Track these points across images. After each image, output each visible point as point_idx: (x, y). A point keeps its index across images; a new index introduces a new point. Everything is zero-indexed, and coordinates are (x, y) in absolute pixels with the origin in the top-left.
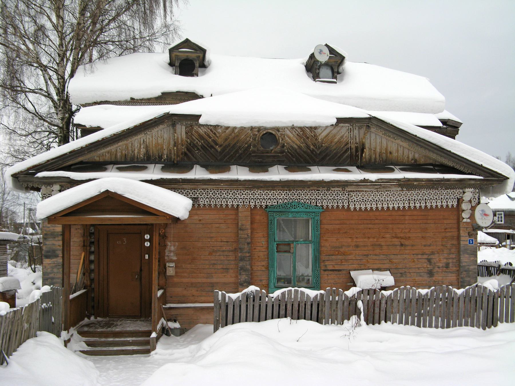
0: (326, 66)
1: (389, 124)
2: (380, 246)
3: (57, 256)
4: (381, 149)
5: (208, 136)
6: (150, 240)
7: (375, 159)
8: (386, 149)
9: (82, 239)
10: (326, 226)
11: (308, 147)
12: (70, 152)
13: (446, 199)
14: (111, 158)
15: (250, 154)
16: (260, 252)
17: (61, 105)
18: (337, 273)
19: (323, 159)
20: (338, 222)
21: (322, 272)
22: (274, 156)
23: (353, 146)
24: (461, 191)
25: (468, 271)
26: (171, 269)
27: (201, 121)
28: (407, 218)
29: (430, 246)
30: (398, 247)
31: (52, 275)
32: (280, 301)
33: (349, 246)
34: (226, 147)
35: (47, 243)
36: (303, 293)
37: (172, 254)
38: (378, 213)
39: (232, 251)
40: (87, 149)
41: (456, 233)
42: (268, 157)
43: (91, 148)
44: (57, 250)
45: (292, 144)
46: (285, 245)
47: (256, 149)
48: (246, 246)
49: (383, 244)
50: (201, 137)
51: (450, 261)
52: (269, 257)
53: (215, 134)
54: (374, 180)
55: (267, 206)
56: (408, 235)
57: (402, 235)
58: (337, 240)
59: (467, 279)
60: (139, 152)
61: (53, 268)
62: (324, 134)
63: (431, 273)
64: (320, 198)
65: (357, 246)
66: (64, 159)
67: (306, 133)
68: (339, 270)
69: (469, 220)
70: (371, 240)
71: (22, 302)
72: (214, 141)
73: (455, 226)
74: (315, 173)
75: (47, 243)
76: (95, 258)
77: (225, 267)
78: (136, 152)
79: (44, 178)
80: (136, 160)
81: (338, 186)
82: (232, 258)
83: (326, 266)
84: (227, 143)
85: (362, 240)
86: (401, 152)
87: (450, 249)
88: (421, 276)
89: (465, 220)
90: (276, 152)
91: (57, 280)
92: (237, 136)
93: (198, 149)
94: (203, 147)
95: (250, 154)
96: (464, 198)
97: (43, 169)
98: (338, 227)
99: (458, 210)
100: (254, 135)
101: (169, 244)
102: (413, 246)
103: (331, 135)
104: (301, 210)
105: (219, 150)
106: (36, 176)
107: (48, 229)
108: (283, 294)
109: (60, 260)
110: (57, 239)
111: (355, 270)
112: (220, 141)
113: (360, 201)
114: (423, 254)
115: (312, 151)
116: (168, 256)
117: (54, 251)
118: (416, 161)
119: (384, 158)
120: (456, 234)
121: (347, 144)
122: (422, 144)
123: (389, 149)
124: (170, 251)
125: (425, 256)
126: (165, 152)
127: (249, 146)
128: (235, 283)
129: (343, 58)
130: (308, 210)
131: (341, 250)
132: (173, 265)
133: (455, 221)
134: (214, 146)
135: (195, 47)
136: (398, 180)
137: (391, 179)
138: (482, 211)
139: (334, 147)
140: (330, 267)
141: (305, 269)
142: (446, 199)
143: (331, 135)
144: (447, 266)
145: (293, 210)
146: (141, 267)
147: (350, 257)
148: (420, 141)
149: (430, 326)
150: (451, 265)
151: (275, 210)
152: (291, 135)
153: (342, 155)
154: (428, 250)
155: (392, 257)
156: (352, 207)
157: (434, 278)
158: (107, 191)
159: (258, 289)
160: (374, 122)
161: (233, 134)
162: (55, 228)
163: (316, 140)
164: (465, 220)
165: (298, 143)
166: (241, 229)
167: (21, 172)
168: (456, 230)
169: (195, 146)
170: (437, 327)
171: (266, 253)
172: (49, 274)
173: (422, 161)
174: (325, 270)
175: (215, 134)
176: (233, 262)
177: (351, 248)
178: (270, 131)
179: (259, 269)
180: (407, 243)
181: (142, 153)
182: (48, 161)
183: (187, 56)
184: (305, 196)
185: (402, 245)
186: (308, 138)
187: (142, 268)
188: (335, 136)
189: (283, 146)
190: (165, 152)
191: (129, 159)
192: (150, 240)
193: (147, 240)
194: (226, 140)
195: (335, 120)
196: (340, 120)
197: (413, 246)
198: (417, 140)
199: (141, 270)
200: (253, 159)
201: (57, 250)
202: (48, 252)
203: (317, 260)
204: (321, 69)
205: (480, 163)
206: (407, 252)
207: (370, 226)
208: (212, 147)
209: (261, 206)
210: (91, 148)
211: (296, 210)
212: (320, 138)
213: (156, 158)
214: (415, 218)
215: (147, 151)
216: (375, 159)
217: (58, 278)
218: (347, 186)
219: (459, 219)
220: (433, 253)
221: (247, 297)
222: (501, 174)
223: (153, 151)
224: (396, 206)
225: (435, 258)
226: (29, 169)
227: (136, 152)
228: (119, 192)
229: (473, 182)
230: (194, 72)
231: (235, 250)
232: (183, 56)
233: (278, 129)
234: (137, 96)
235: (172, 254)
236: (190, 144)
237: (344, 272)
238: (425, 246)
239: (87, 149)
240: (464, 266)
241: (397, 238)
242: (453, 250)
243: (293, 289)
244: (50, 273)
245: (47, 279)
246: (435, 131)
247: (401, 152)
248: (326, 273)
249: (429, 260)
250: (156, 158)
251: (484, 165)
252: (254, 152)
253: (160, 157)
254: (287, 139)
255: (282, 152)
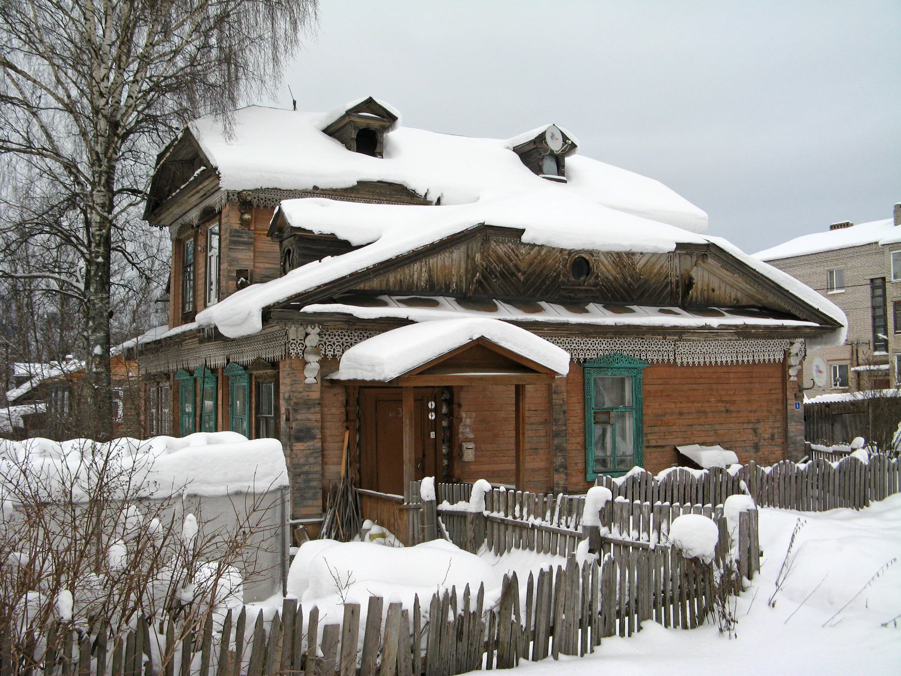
0: (542, 156)
1: (728, 253)
2: (705, 412)
3: (313, 438)
4: (702, 285)
5: (509, 257)
6: (436, 410)
7: (697, 298)
8: (708, 285)
9: (343, 410)
10: (647, 388)
11: (625, 279)
12: (351, 275)
13: (772, 352)
14: (381, 285)
15: (559, 286)
16: (575, 424)
17: (103, 182)
18: (660, 450)
19: (642, 295)
20: (660, 381)
21: (645, 449)
22: (586, 291)
23: (674, 280)
24: (788, 341)
25: (794, 443)
26: (469, 451)
27: (525, 238)
28: (732, 375)
29: (755, 412)
30: (724, 415)
31: (306, 468)
32: (666, 483)
33: (672, 414)
34: (531, 274)
35: (299, 417)
36: (687, 473)
37: (468, 430)
38: (701, 370)
39: (542, 423)
40: (373, 272)
41: (781, 395)
42: (581, 291)
43: (379, 269)
44: (313, 428)
45: (607, 274)
46: (603, 413)
47: (565, 280)
48: (562, 416)
49: (708, 410)
50: (500, 259)
51: (776, 430)
52: (586, 432)
53: (517, 255)
54: (716, 326)
55: (585, 359)
56: (734, 398)
57: (727, 398)
58: (660, 405)
59: (795, 453)
60: (419, 278)
61: (307, 457)
62: (642, 262)
63: (756, 447)
64: (644, 349)
65: (681, 414)
66: (340, 285)
67: (623, 259)
68: (663, 447)
69: (796, 379)
70: (696, 404)
71: (728, 470)
72: (516, 266)
73: (780, 386)
74: (643, 316)
75: (299, 417)
76: (429, 435)
77: (534, 447)
78: (416, 277)
79: (315, 314)
80: (415, 290)
81: (674, 334)
82: (542, 433)
83: (648, 441)
84: (531, 270)
85: (686, 405)
86: (723, 289)
87: (775, 416)
88: (747, 451)
89: (792, 379)
90: (589, 285)
91: (315, 476)
92: (544, 260)
93: (496, 276)
94: (502, 274)
95: (559, 286)
96: (791, 351)
97: (310, 300)
98: (661, 388)
99: (784, 366)
100: (564, 259)
101: (464, 415)
102: (738, 412)
103: (649, 264)
104: (623, 366)
105: (522, 278)
106: (302, 311)
107: (299, 396)
108: (669, 475)
109: (317, 444)
110: (312, 410)
111: (682, 445)
112: (523, 266)
113: (690, 354)
114: (748, 423)
115: (630, 285)
116: (463, 433)
117: (309, 430)
118: (738, 301)
119: (706, 297)
120: (780, 396)
121: (667, 276)
122: (761, 282)
123: (711, 286)
124: (465, 426)
125: (751, 426)
126: (454, 279)
127: (558, 275)
128: (546, 469)
129: (393, 119)
130: (632, 366)
131: (665, 419)
132: (471, 445)
133: (779, 380)
134: (516, 272)
135: (381, 111)
136: (736, 326)
137: (729, 326)
138: (817, 367)
139: (653, 281)
140: (653, 443)
141: (627, 447)
142: (772, 352)
143: (649, 264)
144: (772, 438)
145: (616, 365)
146: (424, 451)
147: (675, 428)
148: (758, 277)
149: (808, 510)
150: (776, 436)
151: (596, 365)
152: (606, 262)
153: (662, 291)
154: (753, 417)
155: (717, 427)
156: (679, 361)
157: (760, 453)
158: (482, 339)
159: (643, 470)
160: (713, 250)
161: (539, 258)
162: (311, 393)
163: (634, 269)
164: (792, 379)
165: (614, 273)
166: (555, 392)
167: (278, 303)
168: (780, 391)
169: (492, 272)
170: (814, 510)
171: (581, 425)
172: (301, 466)
173: (744, 301)
174: (648, 447)
175: (517, 255)
176: (543, 439)
177: (674, 417)
178: (583, 255)
179: (574, 447)
180: (733, 408)
181: (423, 279)
182: (319, 287)
183: (368, 124)
184: (628, 347)
185: (727, 411)
186: (625, 266)
187: (426, 453)
188: (654, 265)
189: (597, 277)
190: (454, 279)
191: (405, 289)
192: (436, 410)
193: (431, 410)
194: (531, 264)
195: (675, 246)
196: (680, 246)
197: (738, 412)
198: (755, 276)
199: (424, 455)
200: (563, 293)
201: (313, 428)
202: (300, 431)
203: (639, 433)
204: (545, 160)
205: (816, 307)
206: (733, 420)
207: (695, 386)
208: (513, 274)
209: (579, 359)
210: (379, 269)
211: (619, 365)
212: (639, 266)
213: (441, 288)
214: (740, 375)
215: (430, 276)
216: (697, 298)
217: (315, 473)
218: (684, 333)
219: (785, 376)
220: (758, 422)
221: (633, 478)
222: (836, 321)
223: (438, 276)
224: (724, 360)
225: (761, 427)
226: (290, 299)
227: (416, 277)
228: (495, 339)
229: (808, 330)
230: (378, 150)
231: (546, 422)
232: (362, 123)
233: (591, 253)
234: (323, 184)
235: (468, 430)
236: (486, 269)
237: (667, 449)
238: (751, 412)
239: (373, 272)
240: (792, 437)
241: (723, 402)
242: (779, 417)
243: (678, 468)
244: (304, 465)
245: (299, 475)
246: (774, 266)
247: (723, 289)
248: (649, 450)
249: (755, 431)
250: (441, 288)
251: (821, 310)
252: (563, 283)
253: (448, 287)
254: (602, 267)
255: (596, 285)
